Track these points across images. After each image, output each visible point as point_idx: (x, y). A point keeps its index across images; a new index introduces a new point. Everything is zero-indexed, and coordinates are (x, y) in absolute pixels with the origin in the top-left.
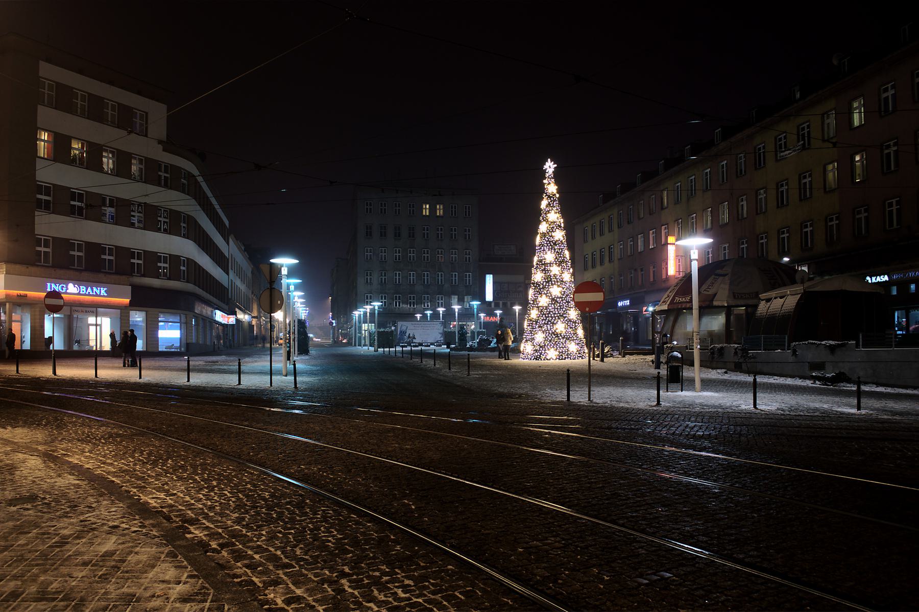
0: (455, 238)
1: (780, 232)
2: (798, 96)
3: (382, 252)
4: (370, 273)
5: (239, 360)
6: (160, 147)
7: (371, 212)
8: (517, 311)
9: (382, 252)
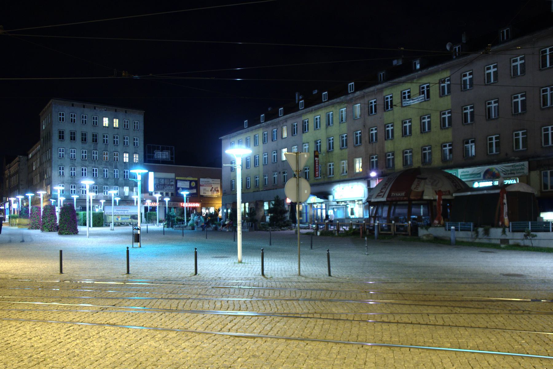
0: (127, 144)
1: (404, 152)
2: (418, 67)
3: (72, 152)
5: (328, 251)
9: (72, 152)
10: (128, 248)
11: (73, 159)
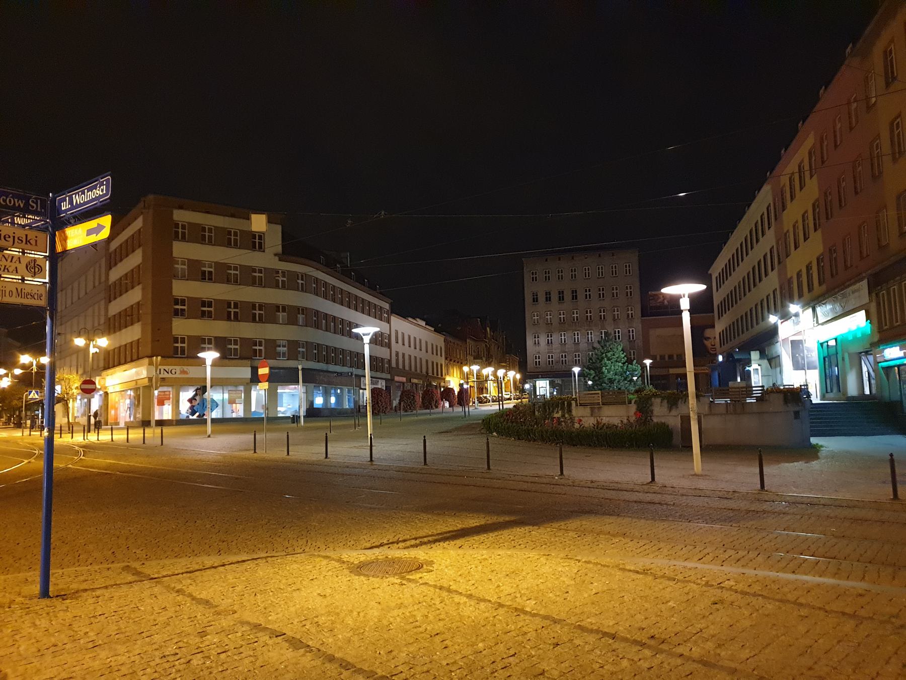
4: (551, 335)
6: (277, 258)
7: (536, 280)
8: (648, 365)
10: (326, 434)
11: (549, 324)
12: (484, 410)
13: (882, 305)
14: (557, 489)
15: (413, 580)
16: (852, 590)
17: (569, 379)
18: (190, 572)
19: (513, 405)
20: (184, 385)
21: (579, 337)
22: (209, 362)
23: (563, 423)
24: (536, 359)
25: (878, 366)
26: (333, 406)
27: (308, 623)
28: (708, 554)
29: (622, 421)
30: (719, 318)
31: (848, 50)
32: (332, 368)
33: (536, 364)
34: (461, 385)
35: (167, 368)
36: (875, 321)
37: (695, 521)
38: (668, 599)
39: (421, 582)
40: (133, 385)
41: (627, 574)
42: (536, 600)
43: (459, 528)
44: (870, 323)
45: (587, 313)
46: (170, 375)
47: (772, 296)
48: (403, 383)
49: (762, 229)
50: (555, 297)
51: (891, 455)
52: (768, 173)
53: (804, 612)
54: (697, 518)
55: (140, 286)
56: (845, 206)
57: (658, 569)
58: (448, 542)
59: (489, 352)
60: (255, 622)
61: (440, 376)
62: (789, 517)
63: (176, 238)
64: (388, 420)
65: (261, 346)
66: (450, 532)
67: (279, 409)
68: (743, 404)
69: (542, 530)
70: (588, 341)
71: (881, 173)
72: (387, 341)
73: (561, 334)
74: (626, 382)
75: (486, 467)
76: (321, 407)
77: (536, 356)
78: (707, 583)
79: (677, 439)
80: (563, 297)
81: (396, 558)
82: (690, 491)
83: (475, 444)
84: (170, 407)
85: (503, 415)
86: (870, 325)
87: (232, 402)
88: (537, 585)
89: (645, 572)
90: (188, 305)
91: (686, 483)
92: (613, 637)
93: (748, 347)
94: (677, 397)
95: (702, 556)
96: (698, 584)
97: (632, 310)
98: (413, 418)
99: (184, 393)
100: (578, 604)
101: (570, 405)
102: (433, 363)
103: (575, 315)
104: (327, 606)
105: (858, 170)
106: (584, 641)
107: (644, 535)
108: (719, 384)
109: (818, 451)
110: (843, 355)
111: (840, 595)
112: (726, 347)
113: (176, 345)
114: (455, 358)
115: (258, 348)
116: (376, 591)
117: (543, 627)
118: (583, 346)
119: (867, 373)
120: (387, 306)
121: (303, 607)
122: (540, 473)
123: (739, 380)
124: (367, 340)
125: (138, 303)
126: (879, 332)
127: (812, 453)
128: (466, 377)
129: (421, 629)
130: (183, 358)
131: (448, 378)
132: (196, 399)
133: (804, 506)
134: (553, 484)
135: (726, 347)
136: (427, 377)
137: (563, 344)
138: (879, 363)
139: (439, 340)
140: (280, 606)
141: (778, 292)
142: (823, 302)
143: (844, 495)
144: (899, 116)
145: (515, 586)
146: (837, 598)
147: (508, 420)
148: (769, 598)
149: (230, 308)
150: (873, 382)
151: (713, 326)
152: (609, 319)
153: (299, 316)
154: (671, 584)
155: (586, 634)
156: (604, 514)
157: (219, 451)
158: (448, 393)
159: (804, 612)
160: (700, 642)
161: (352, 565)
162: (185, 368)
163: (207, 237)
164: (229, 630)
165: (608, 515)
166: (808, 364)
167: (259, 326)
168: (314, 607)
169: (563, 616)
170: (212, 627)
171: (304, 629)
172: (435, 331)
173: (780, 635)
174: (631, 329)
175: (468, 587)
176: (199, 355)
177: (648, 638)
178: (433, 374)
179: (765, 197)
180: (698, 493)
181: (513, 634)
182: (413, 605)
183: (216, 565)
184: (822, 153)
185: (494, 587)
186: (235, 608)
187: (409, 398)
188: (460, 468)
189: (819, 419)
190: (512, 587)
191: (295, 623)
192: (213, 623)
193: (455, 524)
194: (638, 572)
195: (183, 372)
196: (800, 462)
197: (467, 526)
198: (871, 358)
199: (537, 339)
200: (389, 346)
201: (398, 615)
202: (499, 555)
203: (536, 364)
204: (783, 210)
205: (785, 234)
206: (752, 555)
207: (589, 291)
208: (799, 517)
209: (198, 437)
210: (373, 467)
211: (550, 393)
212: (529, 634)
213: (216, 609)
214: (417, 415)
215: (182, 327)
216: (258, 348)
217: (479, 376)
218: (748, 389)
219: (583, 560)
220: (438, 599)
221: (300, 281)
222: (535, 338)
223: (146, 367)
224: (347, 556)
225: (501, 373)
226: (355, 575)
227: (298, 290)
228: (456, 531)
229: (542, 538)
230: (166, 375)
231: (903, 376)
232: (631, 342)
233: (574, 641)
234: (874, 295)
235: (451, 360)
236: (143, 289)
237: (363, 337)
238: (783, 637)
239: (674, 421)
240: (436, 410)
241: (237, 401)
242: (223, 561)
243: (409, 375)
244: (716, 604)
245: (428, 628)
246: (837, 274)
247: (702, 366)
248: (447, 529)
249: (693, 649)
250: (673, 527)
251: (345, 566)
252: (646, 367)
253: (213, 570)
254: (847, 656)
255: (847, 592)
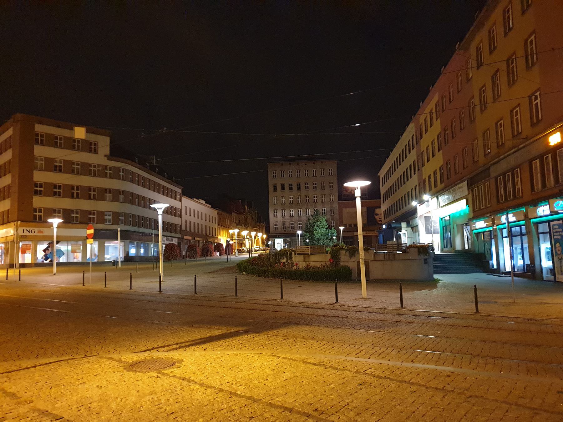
6: (106, 158)
8: (342, 230)
11: (283, 204)
12: (242, 258)
13: (475, 196)
14: (277, 308)
15: (166, 373)
16: (443, 372)
17: (295, 238)
18: (9, 372)
19: (258, 254)
20: (42, 241)
21: (301, 212)
22: (55, 226)
23: (287, 266)
24: (275, 225)
25: (472, 232)
26: (142, 255)
27: (83, 409)
28: (363, 350)
29: (322, 264)
30: (384, 203)
31: (457, 46)
32: (142, 230)
33: (275, 229)
34: (228, 242)
35: (28, 229)
36: (471, 205)
37: (358, 329)
38: (331, 382)
39: (171, 375)
40: (4, 240)
41: (308, 365)
42: (245, 386)
43: (207, 336)
44: (468, 207)
45: (314, 198)
46: (30, 234)
47: (414, 190)
48: (190, 240)
49: (409, 149)
50: (287, 187)
51: (475, 286)
52: (413, 116)
53: (414, 388)
54: (359, 326)
55: (10, 174)
56: (455, 137)
57: (328, 362)
58: (197, 346)
59: (246, 221)
60: (45, 409)
61: (214, 236)
62: (415, 325)
63: (37, 142)
64: (176, 264)
65: (94, 215)
66: (201, 339)
67: (106, 256)
68: (394, 255)
69: (261, 336)
70: (307, 215)
71: (474, 119)
72: (179, 213)
73: (291, 210)
74: (328, 240)
75: (234, 294)
76: (134, 255)
77: (275, 224)
78: (357, 371)
79: (354, 276)
80: (292, 187)
81: (159, 358)
82: (359, 308)
83: (228, 279)
84: (30, 255)
85: (252, 261)
86: (468, 208)
87: (74, 251)
88: (249, 375)
89: (319, 364)
90: (44, 187)
91: (357, 303)
92: (291, 411)
93: (399, 220)
94: (354, 252)
95: (359, 352)
96: (352, 372)
97: (324, 197)
98: (194, 263)
99: (41, 246)
100: (272, 387)
101: (291, 254)
102: (210, 227)
103: (299, 199)
104: (100, 395)
105: (462, 117)
106: (271, 414)
107: (325, 338)
108: (383, 241)
109: (437, 283)
110: (453, 225)
111: (437, 375)
112: (387, 220)
113: (35, 214)
114: (224, 225)
115: (92, 216)
116: (138, 383)
117: (246, 405)
118: (304, 218)
119: (466, 236)
120: (179, 191)
121: (83, 396)
122: (269, 298)
123: (395, 239)
124: (160, 212)
125: (9, 185)
126: (473, 212)
127: (433, 284)
128: (232, 237)
129: (162, 410)
130: (77, 223)
131: (219, 237)
132: (48, 250)
133: (424, 318)
134: (275, 305)
135: (387, 220)
136: (206, 237)
137: (292, 217)
138: (473, 230)
139: (214, 213)
140: (67, 396)
141: (418, 187)
142: (443, 194)
143: (449, 310)
144: (484, 86)
145: (234, 376)
146: (434, 378)
147: (253, 264)
148: (393, 380)
149: (74, 190)
150: (470, 241)
151: (380, 207)
152: (319, 201)
153: (120, 196)
154: (335, 372)
155: (273, 409)
156: (303, 324)
157: (60, 284)
158: (219, 247)
159: (414, 388)
160: (346, 412)
161: (127, 364)
162: (41, 229)
163: (58, 143)
164: (23, 416)
165: (304, 325)
166: (434, 230)
167: (93, 202)
168: (91, 396)
169: (261, 397)
170: (11, 414)
171: (79, 413)
172: (211, 207)
173: (396, 405)
174: (332, 208)
175: (202, 378)
176: (49, 220)
177: (313, 411)
178: (210, 235)
179: (411, 130)
180: (363, 310)
181: (225, 411)
182: (161, 392)
183: (29, 366)
184: (443, 106)
185: (219, 377)
186: (33, 399)
187: (193, 250)
188: (218, 295)
189: (439, 263)
190: (231, 377)
191: (73, 409)
192: (13, 410)
193: (206, 333)
194: (315, 364)
195: (40, 232)
196: (426, 290)
197: (213, 335)
198: (469, 227)
199: (276, 213)
200: (181, 216)
201: (149, 400)
202: (228, 355)
203: (275, 229)
204: (421, 139)
205: (422, 153)
206: (389, 350)
207: (308, 185)
208: (420, 325)
209: (47, 275)
210: (161, 295)
211: (283, 247)
212: (235, 411)
213: (19, 400)
214: (197, 261)
215: (39, 202)
216: (92, 216)
217: (239, 236)
218: (399, 245)
219: (282, 357)
220: (180, 387)
221: (121, 174)
222: (275, 212)
223: (13, 228)
224: (125, 358)
225: (253, 234)
226: (127, 371)
227: (120, 179)
228: (205, 338)
229: (260, 341)
230: (28, 234)
231: (486, 238)
232: (332, 216)
233: (265, 415)
234: (470, 190)
235: (222, 226)
236: (13, 176)
237: (158, 210)
238: (399, 406)
239: (352, 265)
240: (212, 257)
241: (77, 251)
242: (35, 363)
243: (194, 235)
244: (361, 385)
245: (167, 409)
246: (450, 177)
247: (374, 231)
248: (200, 337)
249: (341, 418)
250: (344, 332)
251: (121, 365)
252: (341, 231)
253: (26, 370)
254: (435, 418)
255: (441, 374)
